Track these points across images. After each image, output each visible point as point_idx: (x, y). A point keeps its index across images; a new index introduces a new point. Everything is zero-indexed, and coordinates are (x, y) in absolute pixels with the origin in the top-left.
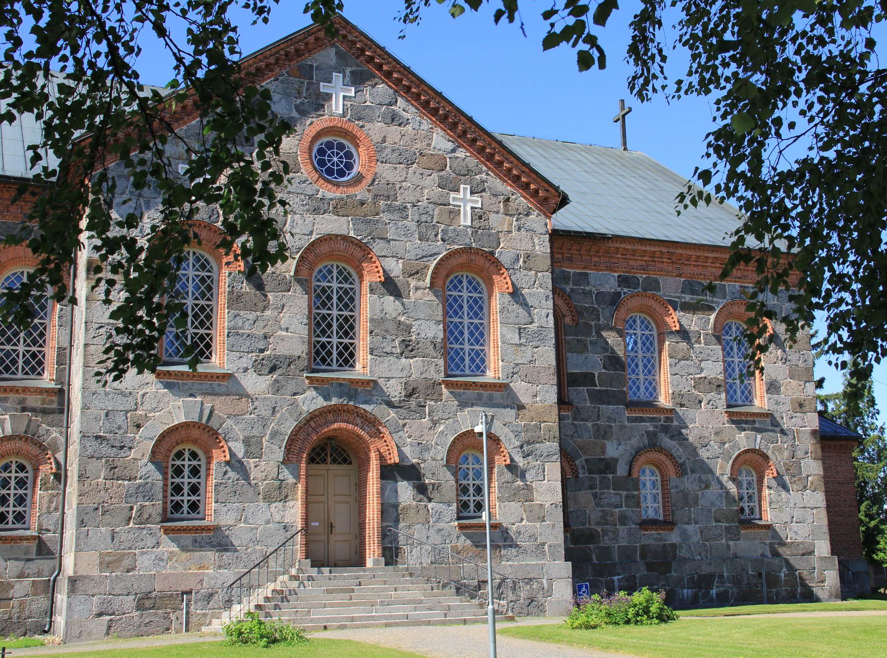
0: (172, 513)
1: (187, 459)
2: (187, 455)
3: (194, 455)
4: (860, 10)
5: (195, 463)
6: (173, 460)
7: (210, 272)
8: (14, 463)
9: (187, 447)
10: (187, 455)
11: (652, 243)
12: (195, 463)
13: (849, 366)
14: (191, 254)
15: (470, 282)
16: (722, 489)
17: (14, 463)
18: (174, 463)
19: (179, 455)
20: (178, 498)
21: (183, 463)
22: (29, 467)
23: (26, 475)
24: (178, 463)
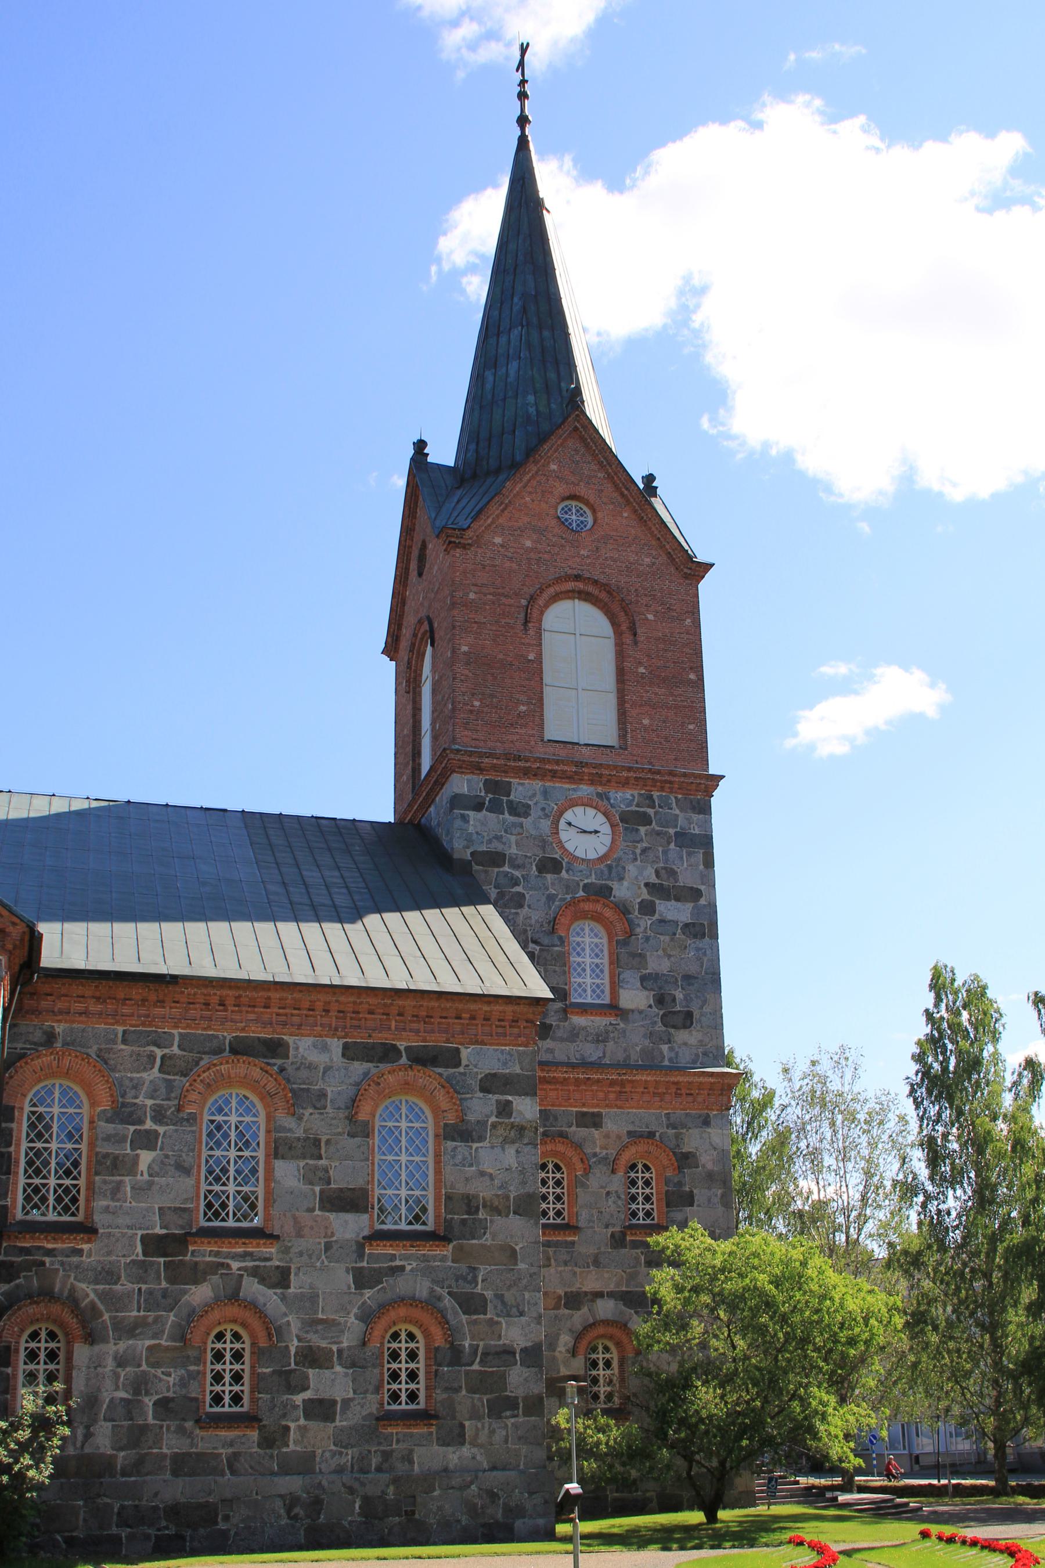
0: (211, 1406)
1: (403, 1341)
2: (228, 1336)
3: (411, 1337)
4: (440, 272)
5: (412, 1345)
6: (389, 1342)
7: (80, 1108)
8: (43, 1329)
9: (403, 1328)
10: (228, 1336)
11: (449, 997)
12: (412, 1345)
13: (725, 1246)
14: (234, 1096)
15: (411, 1109)
16: (70, 1542)
17: (43, 1329)
18: (390, 1345)
19: (220, 1336)
20: (218, 1388)
21: (38, 1345)
22: (61, 1336)
23: (242, 1346)
24: (219, 1346)
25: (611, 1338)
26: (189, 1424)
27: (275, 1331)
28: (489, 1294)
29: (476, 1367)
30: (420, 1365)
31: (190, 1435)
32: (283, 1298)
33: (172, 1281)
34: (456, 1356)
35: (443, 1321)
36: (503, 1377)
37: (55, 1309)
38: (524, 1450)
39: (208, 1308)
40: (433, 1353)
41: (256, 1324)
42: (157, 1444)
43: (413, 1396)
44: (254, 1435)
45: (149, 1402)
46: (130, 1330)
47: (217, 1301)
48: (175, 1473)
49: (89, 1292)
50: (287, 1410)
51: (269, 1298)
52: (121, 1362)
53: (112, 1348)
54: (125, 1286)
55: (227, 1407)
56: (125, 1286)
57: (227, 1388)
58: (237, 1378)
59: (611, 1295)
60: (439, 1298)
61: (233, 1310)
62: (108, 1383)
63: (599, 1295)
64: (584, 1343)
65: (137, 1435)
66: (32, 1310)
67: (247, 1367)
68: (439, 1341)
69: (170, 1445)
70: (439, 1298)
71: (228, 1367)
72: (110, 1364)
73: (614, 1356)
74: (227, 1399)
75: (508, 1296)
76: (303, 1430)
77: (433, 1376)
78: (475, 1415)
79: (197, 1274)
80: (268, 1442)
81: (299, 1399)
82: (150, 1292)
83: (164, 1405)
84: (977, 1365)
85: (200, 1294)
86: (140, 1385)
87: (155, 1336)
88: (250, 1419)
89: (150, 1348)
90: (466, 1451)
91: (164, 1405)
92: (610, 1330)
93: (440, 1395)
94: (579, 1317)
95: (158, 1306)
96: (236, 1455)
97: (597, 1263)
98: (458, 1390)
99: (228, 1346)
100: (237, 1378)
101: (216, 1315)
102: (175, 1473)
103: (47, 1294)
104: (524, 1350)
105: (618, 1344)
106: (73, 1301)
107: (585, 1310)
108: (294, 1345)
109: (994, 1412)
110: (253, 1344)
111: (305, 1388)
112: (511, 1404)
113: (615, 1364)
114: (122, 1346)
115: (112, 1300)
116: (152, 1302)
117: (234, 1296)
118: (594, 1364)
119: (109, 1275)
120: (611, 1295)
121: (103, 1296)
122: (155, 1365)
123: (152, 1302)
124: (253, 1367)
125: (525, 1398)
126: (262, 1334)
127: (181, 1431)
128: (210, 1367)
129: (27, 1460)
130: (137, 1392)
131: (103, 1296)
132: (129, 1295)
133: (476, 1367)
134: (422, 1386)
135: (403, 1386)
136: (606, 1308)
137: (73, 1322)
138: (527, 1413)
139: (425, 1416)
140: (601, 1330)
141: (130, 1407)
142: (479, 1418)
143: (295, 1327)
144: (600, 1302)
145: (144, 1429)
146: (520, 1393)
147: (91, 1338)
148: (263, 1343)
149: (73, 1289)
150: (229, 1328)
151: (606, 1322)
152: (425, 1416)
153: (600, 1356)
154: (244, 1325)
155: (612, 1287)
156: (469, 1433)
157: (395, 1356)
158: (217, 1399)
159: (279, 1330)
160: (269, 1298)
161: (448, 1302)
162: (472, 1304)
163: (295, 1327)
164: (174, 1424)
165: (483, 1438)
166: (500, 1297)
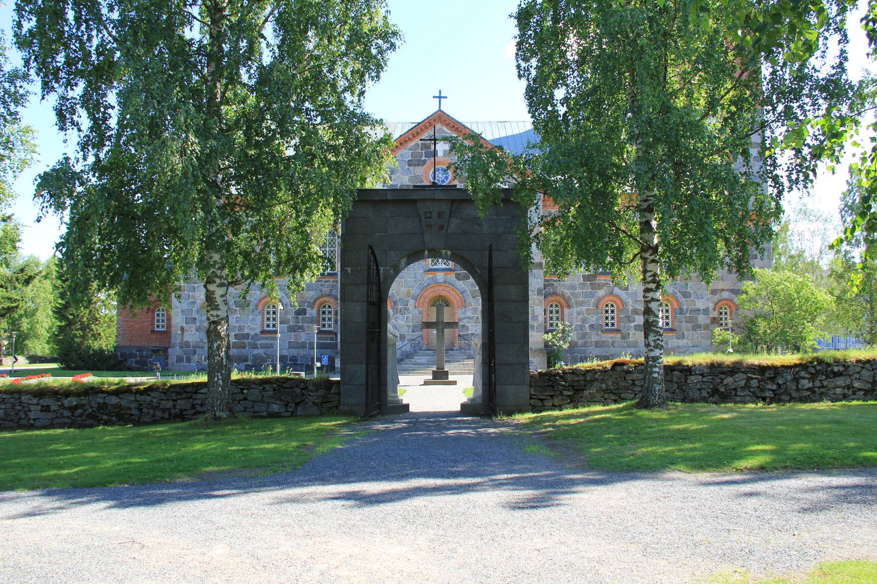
3: (612, 306)
9: (610, 304)
25: (727, 305)
26: (599, 332)
27: (623, 303)
28: (692, 292)
29: (688, 315)
30: (615, 315)
31: (600, 335)
32: (627, 294)
33: (592, 289)
34: (681, 311)
35: (677, 301)
36: (697, 318)
37: (558, 298)
38: (703, 341)
39: (604, 297)
40: (674, 310)
41: (619, 302)
42: (590, 337)
43: (613, 324)
44: (619, 335)
45: (587, 325)
46: (581, 304)
47: (606, 295)
48: (596, 346)
49: (567, 293)
50: (629, 328)
51: (622, 294)
52: (578, 314)
53: (575, 310)
54: (578, 291)
55: (610, 327)
56: (578, 291)
57: (610, 321)
58: (613, 318)
59: (727, 290)
60: (676, 293)
61: (611, 298)
62: (575, 320)
63: (723, 290)
64: (718, 306)
65: (584, 336)
66: (551, 298)
67: (616, 315)
68: (676, 306)
69: (594, 338)
70: (676, 293)
71: (610, 315)
72: (575, 314)
73: (728, 311)
74: (271, 326)
75: (698, 292)
76: (634, 334)
77: (674, 318)
78: (688, 330)
79: (600, 287)
80: (623, 338)
81: (632, 325)
82: (586, 292)
83: (592, 326)
84: (864, 316)
85: (601, 293)
86: (584, 321)
87: (588, 306)
88: (618, 331)
89: (587, 309)
90: (685, 341)
91: (592, 326)
92: (727, 302)
93: (676, 324)
94: (716, 298)
95: (588, 297)
96: (614, 341)
97: (722, 279)
98: (682, 322)
99: (609, 308)
100: (613, 318)
101: (606, 299)
102: (596, 346)
103: (555, 294)
104: (703, 309)
105: (730, 307)
106: (563, 296)
107: (718, 295)
108: (630, 308)
109: (870, 333)
110: (618, 308)
111: (634, 322)
112: (699, 326)
113: (728, 313)
114: (578, 309)
115: (575, 295)
116: (587, 295)
117: (611, 293)
118: (721, 313)
119: (573, 287)
120: (727, 290)
121: (572, 294)
122: (589, 314)
123: (587, 295)
124: (617, 315)
125: (704, 325)
126: (620, 305)
127: (597, 334)
128: (615, 315)
129: (561, 342)
130: (583, 322)
131: (572, 294)
132: (579, 293)
133: (688, 315)
134: (670, 321)
135: (610, 321)
136: (726, 295)
137: (563, 302)
138: (704, 330)
139: (672, 330)
140: (724, 302)
141: (582, 327)
142: (689, 331)
143: (631, 303)
144: (723, 293)
145: (586, 334)
146: (702, 323)
147: (569, 307)
148: (621, 308)
149: (563, 292)
150: (610, 304)
151: (726, 300)
152: (672, 330)
153: (723, 311)
154: (615, 302)
155: (728, 288)
156: (686, 335)
157: (607, 312)
158: (607, 324)
159: (626, 303)
160: (622, 294)
161: (678, 294)
162: (686, 295)
163: (631, 303)
164: (595, 332)
165: (690, 337)
166: (695, 293)
